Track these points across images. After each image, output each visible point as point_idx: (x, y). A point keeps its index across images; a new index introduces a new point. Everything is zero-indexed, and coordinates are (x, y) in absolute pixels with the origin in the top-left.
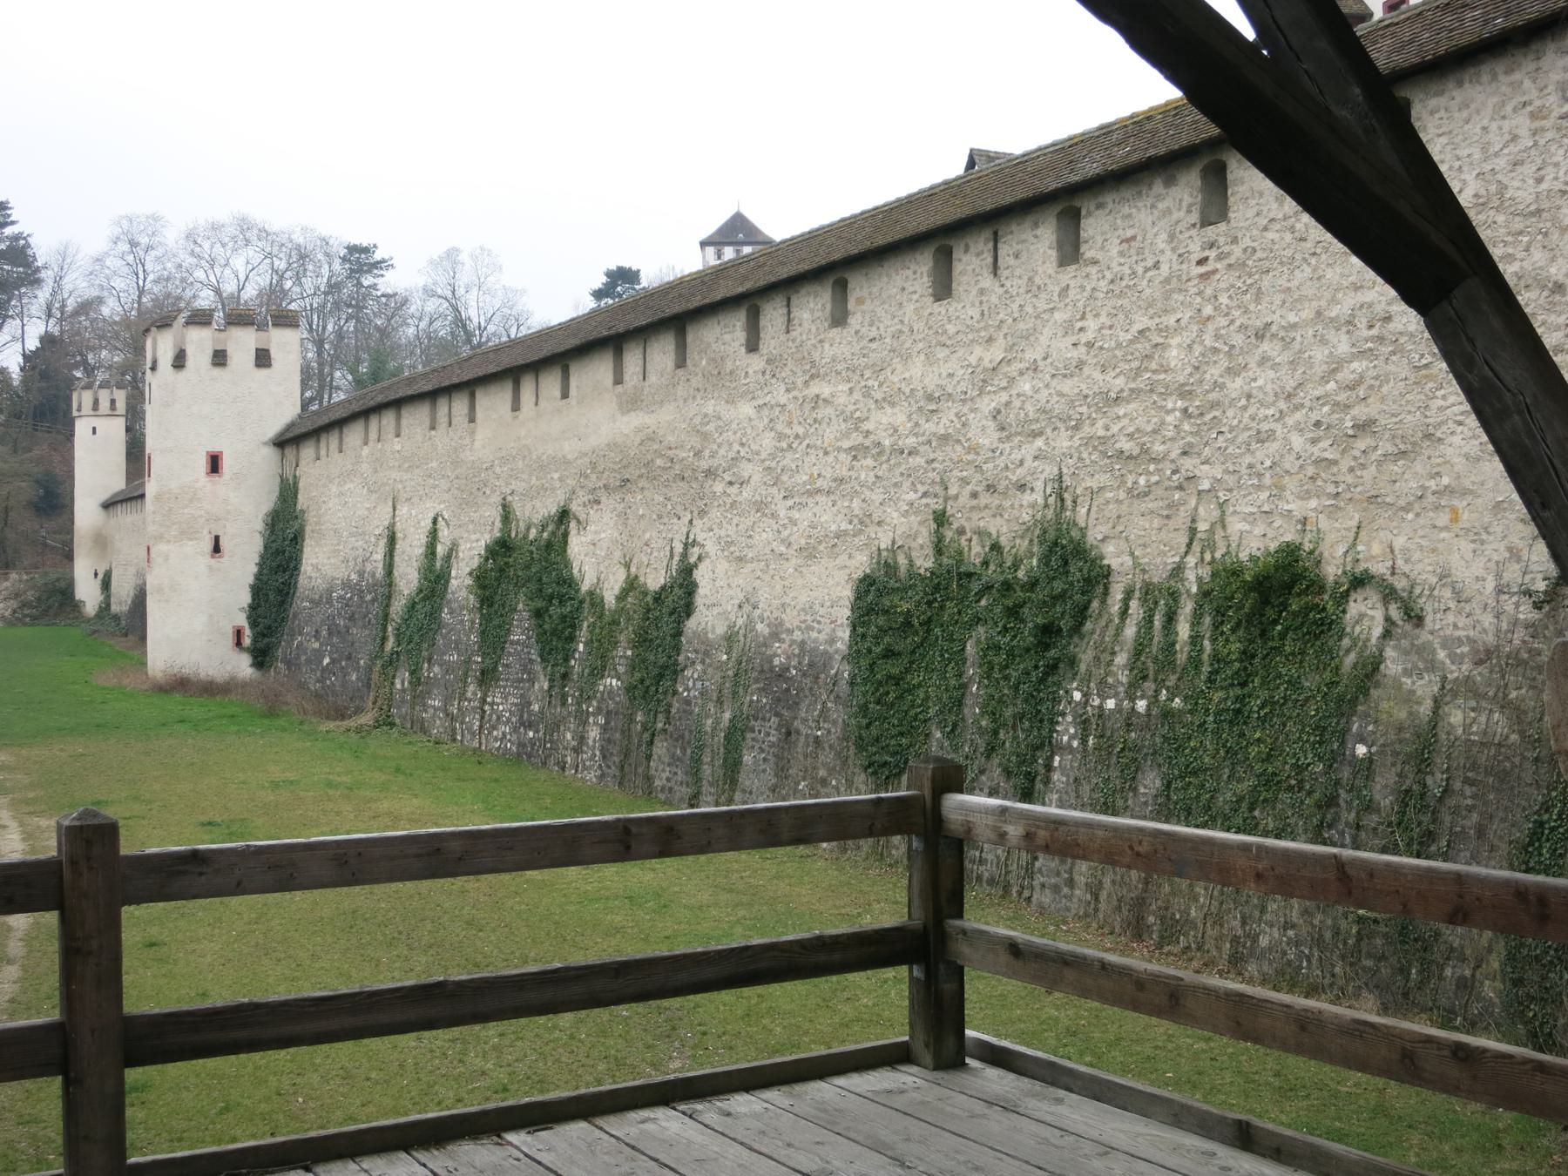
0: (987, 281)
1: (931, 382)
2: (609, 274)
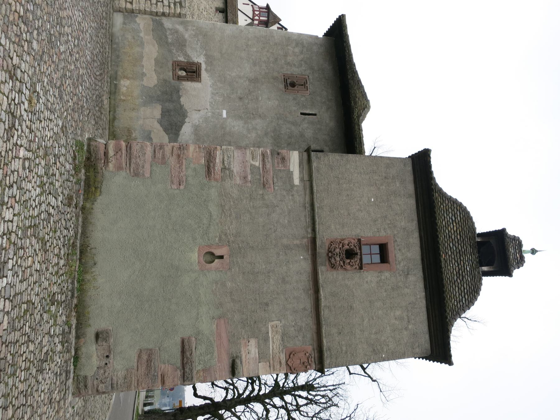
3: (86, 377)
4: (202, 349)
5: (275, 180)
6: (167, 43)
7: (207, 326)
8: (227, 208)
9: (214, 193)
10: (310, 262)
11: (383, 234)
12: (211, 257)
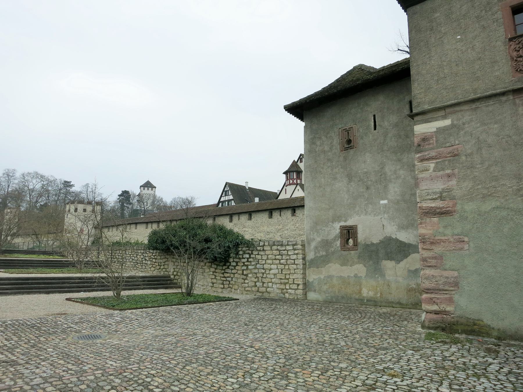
0: (279, 217)
1: (268, 230)
2: (232, 189)
5: (448, 145)
6: (326, 256)
8: (485, 192)
9: (470, 207)
11: (499, 15)
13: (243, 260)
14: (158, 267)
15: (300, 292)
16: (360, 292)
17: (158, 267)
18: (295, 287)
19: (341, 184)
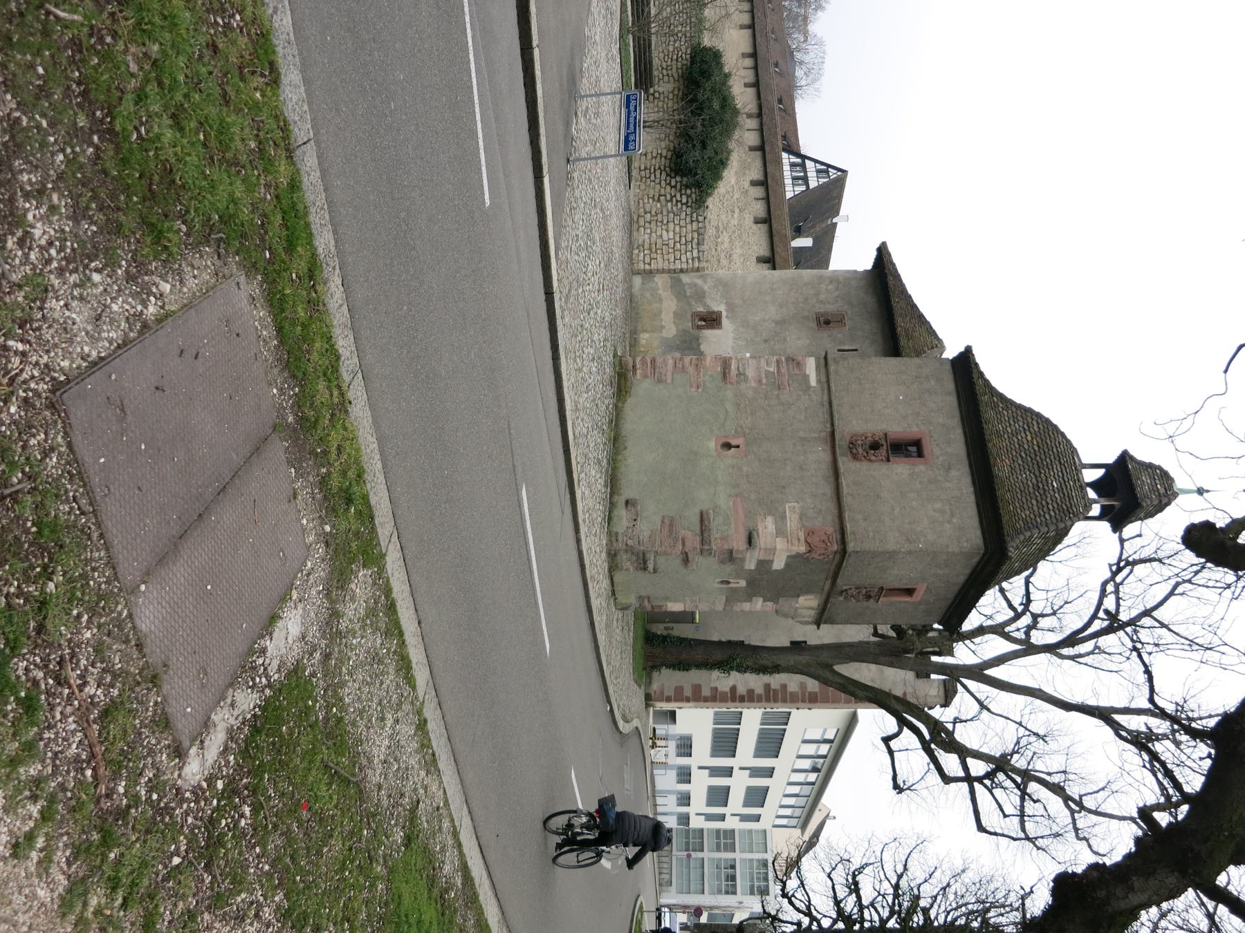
1: (735, 256)
3: (617, 534)
4: (719, 520)
7: (723, 502)
9: (729, 394)
10: (829, 452)
11: (915, 429)
12: (728, 446)
13: (678, 195)
14: (664, 65)
15: (641, 266)
16: (645, 331)
17: (664, 65)
18: (647, 260)
19: (773, 312)
